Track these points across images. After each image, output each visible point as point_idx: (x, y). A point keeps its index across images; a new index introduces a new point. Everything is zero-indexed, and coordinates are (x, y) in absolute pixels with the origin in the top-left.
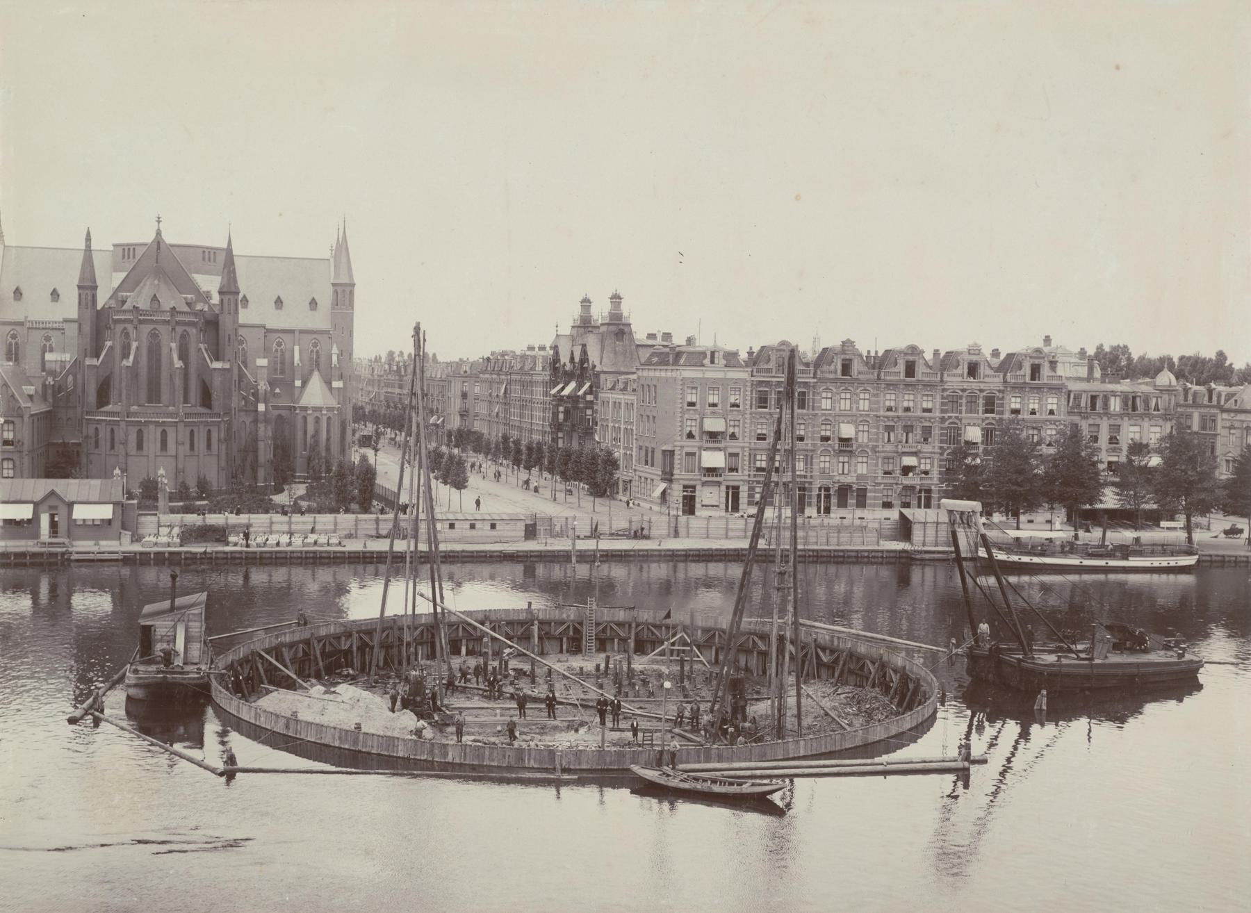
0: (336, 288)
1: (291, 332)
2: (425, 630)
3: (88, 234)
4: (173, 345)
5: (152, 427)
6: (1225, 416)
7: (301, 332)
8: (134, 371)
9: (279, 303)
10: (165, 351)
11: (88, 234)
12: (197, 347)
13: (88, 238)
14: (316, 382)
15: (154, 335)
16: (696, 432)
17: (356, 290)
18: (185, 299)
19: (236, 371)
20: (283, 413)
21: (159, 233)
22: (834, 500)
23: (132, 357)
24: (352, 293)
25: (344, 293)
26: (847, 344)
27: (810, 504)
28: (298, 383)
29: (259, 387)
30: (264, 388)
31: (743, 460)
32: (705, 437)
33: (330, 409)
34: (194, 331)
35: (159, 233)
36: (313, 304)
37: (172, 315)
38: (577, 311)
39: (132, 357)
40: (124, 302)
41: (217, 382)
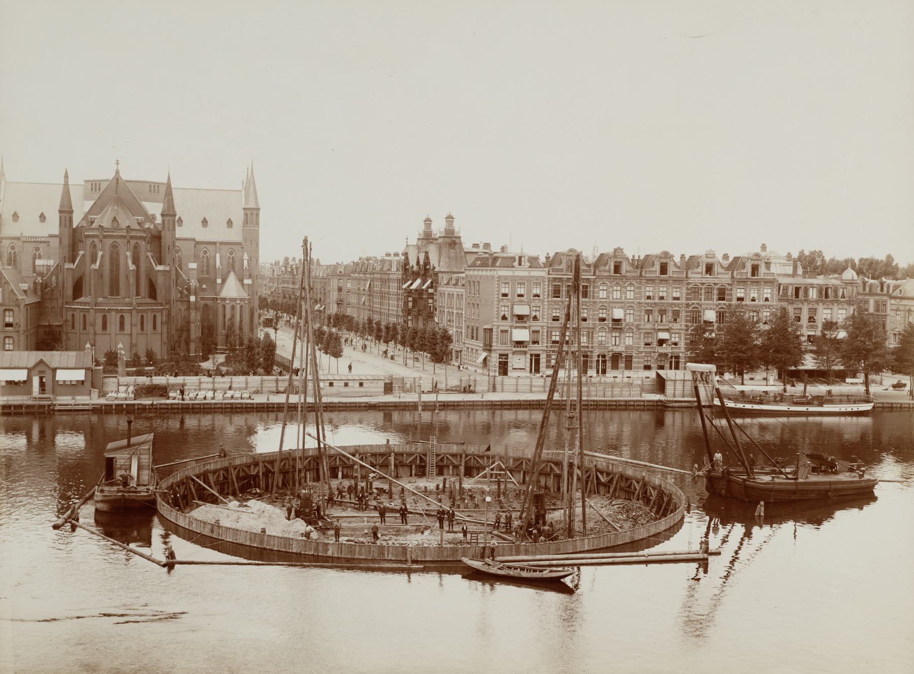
0: (246, 211)
1: (214, 243)
2: (312, 461)
3: (66, 173)
4: (128, 254)
5: (113, 313)
6: (893, 301)
7: (221, 243)
8: (100, 273)
9: (205, 222)
10: (122, 258)
11: (66, 173)
12: (147, 254)
13: (66, 176)
14: (232, 280)
15: (114, 246)
16: (508, 315)
17: (261, 212)
18: (137, 220)
19: (174, 272)
20: (209, 302)
21: (117, 172)
22: (609, 364)
23: (98, 262)
24: (257, 215)
25: (252, 216)
26: (618, 251)
27: (591, 367)
28: (219, 281)
29: (191, 284)
30: (194, 284)
31: (543, 335)
32: (515, 319)
33: (242, 300)
34: (143, 243)
35: (117, 172)
36: (230, 223)
37: (127, 232)
38: (421, 228)
39: (98, 262)
40: (92, 222)
41: (160, 282)
